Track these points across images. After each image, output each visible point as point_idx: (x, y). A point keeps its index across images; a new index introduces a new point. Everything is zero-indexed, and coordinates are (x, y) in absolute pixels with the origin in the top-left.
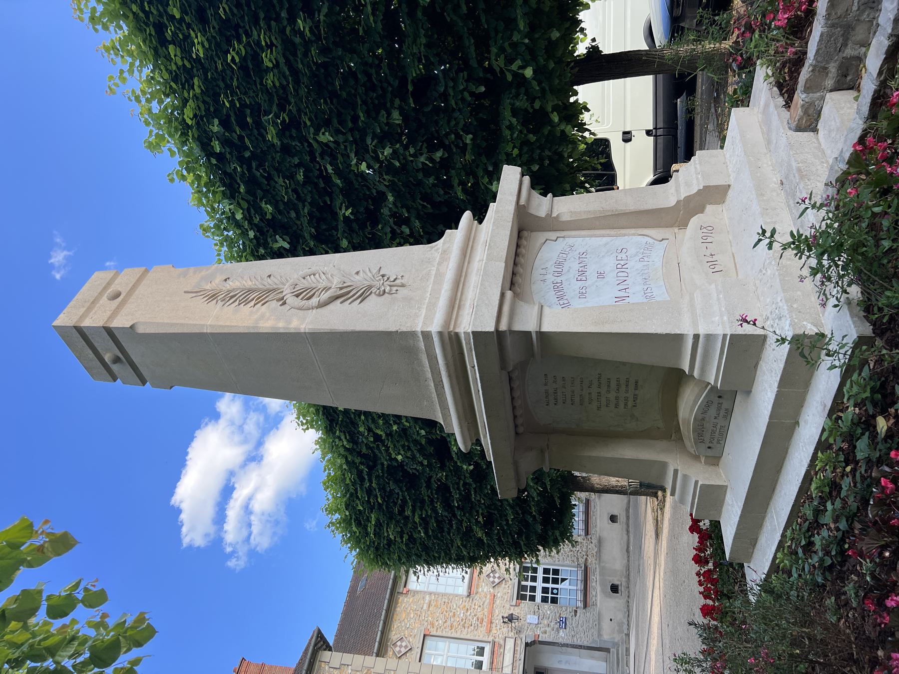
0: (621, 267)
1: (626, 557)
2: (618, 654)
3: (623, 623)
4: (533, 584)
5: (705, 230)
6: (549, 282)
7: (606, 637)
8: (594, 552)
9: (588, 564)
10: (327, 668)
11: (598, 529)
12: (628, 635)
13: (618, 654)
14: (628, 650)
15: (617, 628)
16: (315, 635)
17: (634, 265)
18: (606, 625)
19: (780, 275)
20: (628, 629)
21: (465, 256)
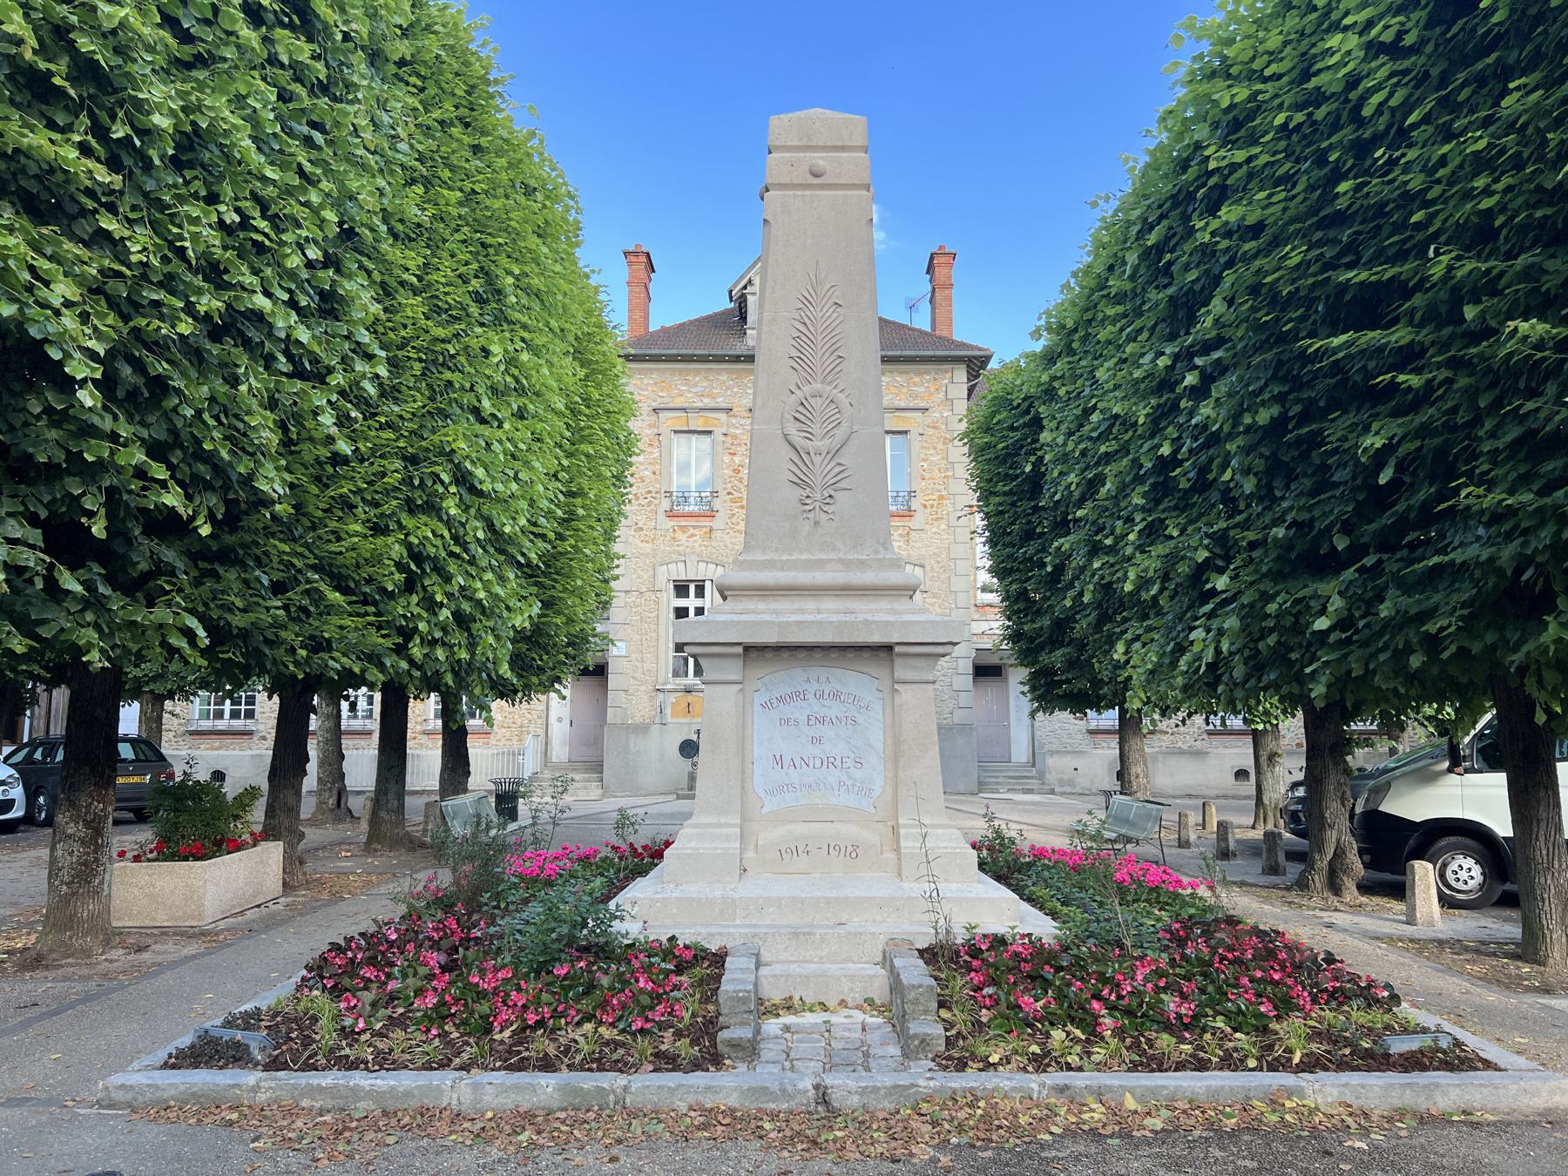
0: (829, 762)
1: (1179, 793)
2: (1027, 777)
3: (1074, 786)
4: (227, 715)
5: (850, 849)
6: (807, 686)
7: (1051, 761)
8: (1180, 744)
9: (1159, 735)
10: (946, 381)
11: (1221, 750)
12: (1052, 792)
13: (1027, 777)
14: (1030, 791)
15: (1065, 777)
16: (981, 353)
17: (833, 775)
18: (1067, 762)
19: (700, 899)
20: (1063, 794)
21: (844, 590)
